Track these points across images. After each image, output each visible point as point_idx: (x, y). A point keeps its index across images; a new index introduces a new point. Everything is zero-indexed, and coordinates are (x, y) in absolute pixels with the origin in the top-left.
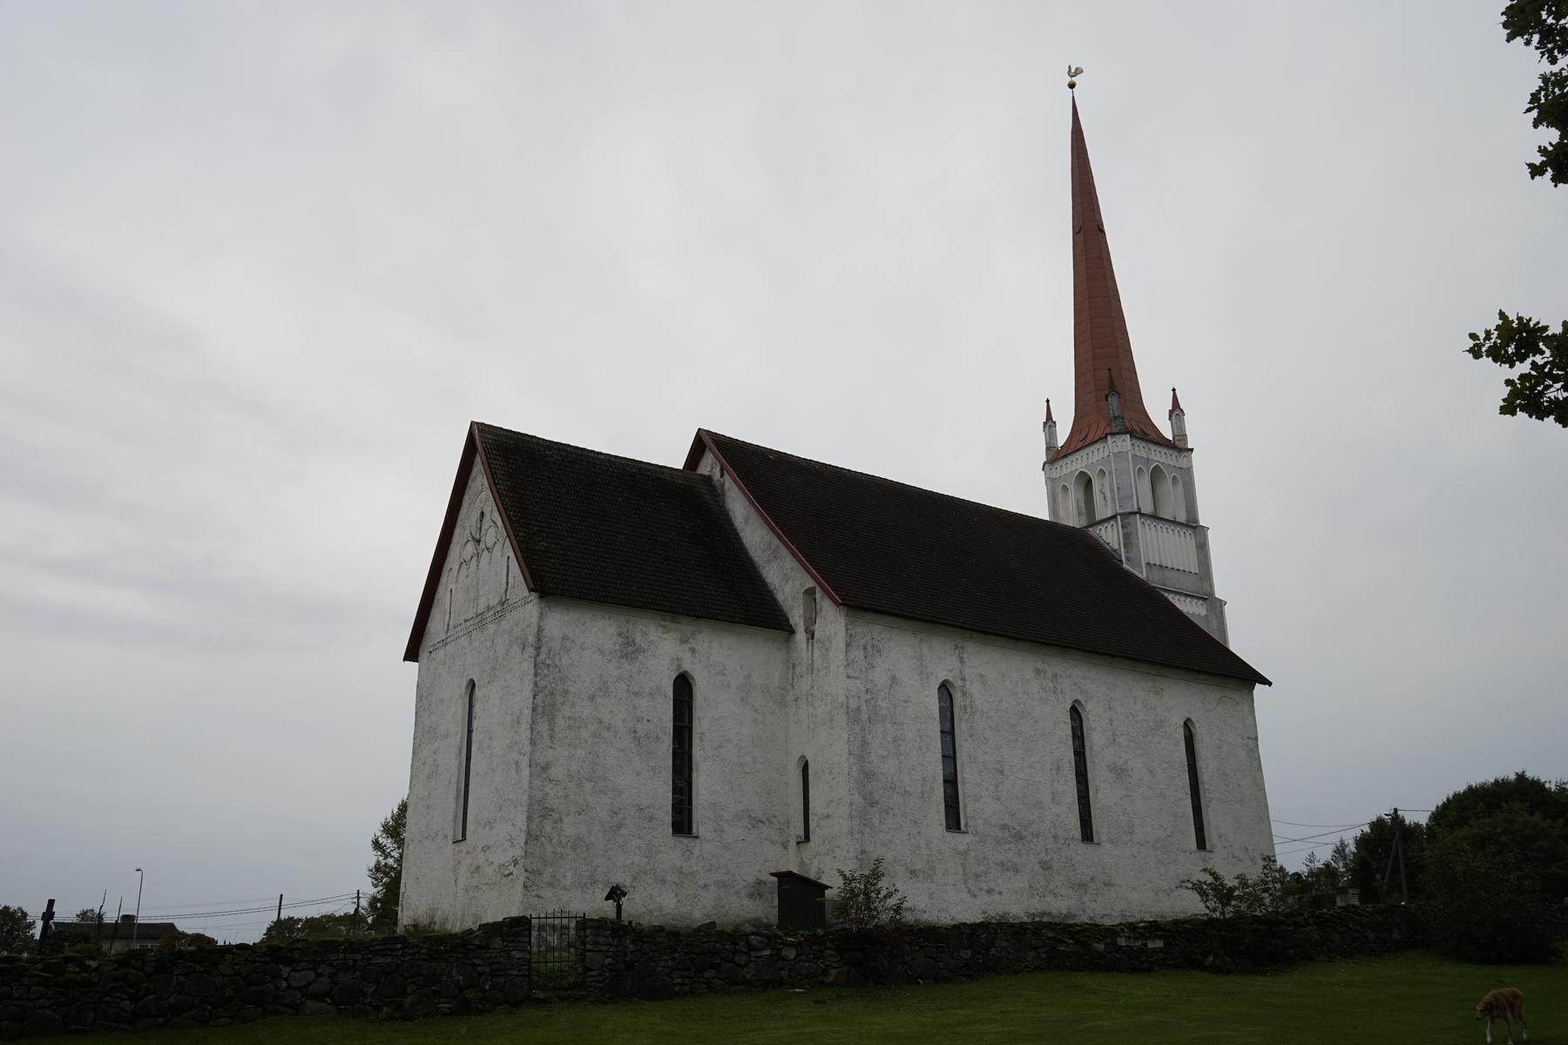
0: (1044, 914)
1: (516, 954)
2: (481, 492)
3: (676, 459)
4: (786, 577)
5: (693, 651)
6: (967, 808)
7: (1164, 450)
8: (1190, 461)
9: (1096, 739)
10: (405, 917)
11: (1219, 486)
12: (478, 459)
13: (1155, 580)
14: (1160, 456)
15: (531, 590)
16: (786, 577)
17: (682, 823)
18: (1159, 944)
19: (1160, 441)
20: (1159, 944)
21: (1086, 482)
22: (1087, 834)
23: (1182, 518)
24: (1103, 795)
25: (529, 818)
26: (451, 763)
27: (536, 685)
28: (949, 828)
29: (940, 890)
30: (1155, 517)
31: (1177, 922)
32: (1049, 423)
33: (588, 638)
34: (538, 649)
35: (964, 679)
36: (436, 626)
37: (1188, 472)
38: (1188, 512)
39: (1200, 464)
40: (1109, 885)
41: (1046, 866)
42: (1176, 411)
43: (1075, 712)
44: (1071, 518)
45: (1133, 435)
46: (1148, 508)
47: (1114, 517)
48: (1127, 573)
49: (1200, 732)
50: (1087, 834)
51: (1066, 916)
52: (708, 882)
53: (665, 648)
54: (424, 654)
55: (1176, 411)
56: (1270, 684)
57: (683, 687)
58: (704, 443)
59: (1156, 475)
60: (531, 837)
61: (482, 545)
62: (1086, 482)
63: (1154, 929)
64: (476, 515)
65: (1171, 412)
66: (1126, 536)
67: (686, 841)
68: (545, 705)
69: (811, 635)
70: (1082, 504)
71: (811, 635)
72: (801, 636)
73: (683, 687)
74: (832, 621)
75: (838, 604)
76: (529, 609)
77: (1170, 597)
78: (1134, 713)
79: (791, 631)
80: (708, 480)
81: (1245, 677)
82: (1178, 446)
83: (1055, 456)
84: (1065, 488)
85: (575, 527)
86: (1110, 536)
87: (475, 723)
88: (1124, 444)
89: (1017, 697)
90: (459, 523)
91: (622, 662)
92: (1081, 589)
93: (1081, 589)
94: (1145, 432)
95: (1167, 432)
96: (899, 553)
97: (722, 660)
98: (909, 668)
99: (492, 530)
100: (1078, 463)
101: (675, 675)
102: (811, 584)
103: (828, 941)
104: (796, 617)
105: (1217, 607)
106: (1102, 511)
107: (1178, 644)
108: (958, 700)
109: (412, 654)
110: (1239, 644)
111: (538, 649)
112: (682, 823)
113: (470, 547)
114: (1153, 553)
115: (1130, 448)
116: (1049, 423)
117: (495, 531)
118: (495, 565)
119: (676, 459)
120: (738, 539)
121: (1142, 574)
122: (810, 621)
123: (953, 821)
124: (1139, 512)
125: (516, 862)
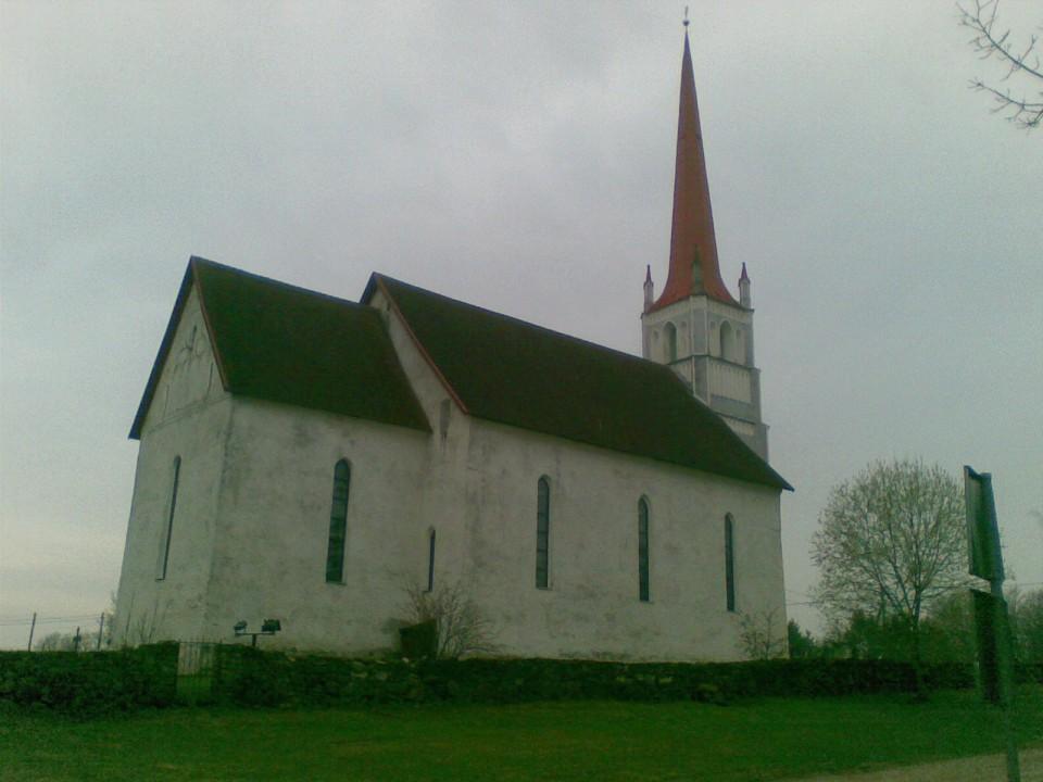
0: (605, 654)
1: (165, 669)
2: (195, 313)
3: (354, 295)
4: (429, 390)
5: (352, 442)
6: (554, 570)
7: (732, 310)
8: (751, 319)
9: (657, 524)
10: (1001, 758)
11: (774, 341)
12: (194, 287)
13: (717, 409)
14: (729, 315)
15: (226, 389)
16: (429, 390)
17: (335, 573)
18: (669, 680)
19: (736, 306)
20: (669, 680)
21: (671, 330)
22: (644, 595)
23: (741, 361)
24: (658, 569)
25: (213, 564)
26: (158, 519)
27: (225, 463)
28: (538, 586)
29: (524, 631)
30: (721, 360)
31: (682, 666)
32: (649, 283)
33: (269, 430)
34: (229, 435)
35: (559, 475)
36: (155, 411)
37: (748, 328)
38: (747, 358)
39: (760, 323)
40: (657, 634)
41: (611, 618)
42: (744, 280)
43: (643, 505)
44: (659, 357)
45: (709, 297)
46: (716, 352)
47: (689, 359)
48: (694, 399)
49: (738, 523)
50: (644, 595)
51: (623, 656)
52: (344, 623)
53: (330, 439)
54: (144, 434)
55: (744, 280)
56: (793, 490)
57: (343, 471)
58: (377, 284)
59: (725, 329)
60: (214, 579)
61: (194, 352)
62: (671, 330)
63: (666, 668)
64: (189, 331)
65: (740, 281)
66: (698, 373)
67: (336, 587)
68: (231, 479)
69: (444, 434)
70: (668, 346)
71: (444, 434)
72: (437, 434)
73: (343, 471)
74: (460, 427)
75: (465, 413)
76: (224, 404)
77: (724, 419)
78: (687, 506)
79: (428, 430)
80: (377, 313)
81: (774, 484)
82: (743, 308)
83: (651, 309)
84: (656, 334)
85: (262, 344)
86: (685, 372)
87: (179, 490)
88: (700, 303)
89: (599, 489)
90: (178, 335)
91: (293, 449)
92: (656, 414)
93: (656, 414)
94: (720, 296)
95: (736, 295)
96: (510, 374)
97: (376, 453)
98: (516, 464)
99: (201, 342)
100: (667, 315)
101: (336, 461)
102: (446, 396)
103: (428, 672)
104: (435, 419)
105: (761, 430)
106: (681, 354)
107: (729, 458)
108: (553, 492)
109: (135, 433)
110: (777, 462)
111: (229, 435)
112: (335, 573)
113: (184, 355)
114: (717, 387)
115: (706, 305)
116: (649, 283)
117: (203, 344)
118: (201, 370)
119: (354, 295)
120: (396, 357)
121: (707, 402)
122: (444, 425)
123: (542, 580)
124: (709, 356)
125: (200, 598)
